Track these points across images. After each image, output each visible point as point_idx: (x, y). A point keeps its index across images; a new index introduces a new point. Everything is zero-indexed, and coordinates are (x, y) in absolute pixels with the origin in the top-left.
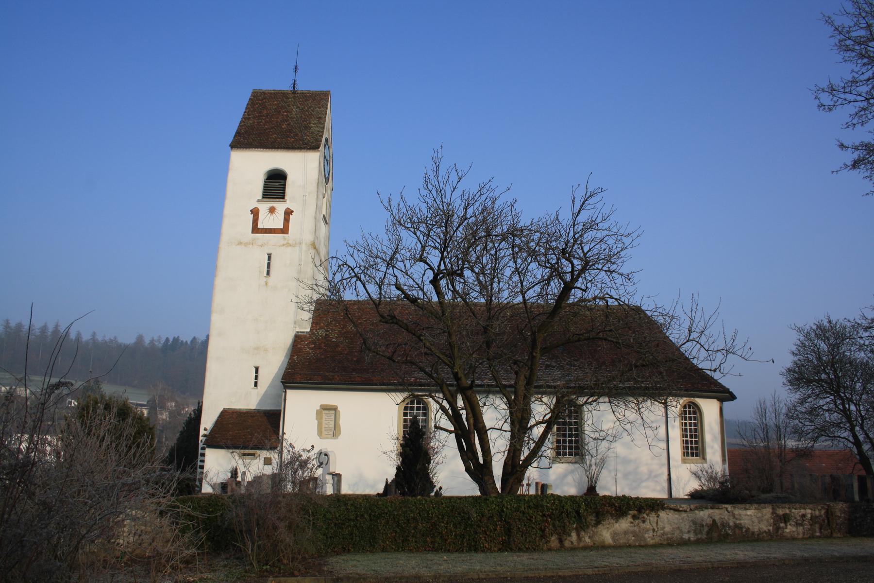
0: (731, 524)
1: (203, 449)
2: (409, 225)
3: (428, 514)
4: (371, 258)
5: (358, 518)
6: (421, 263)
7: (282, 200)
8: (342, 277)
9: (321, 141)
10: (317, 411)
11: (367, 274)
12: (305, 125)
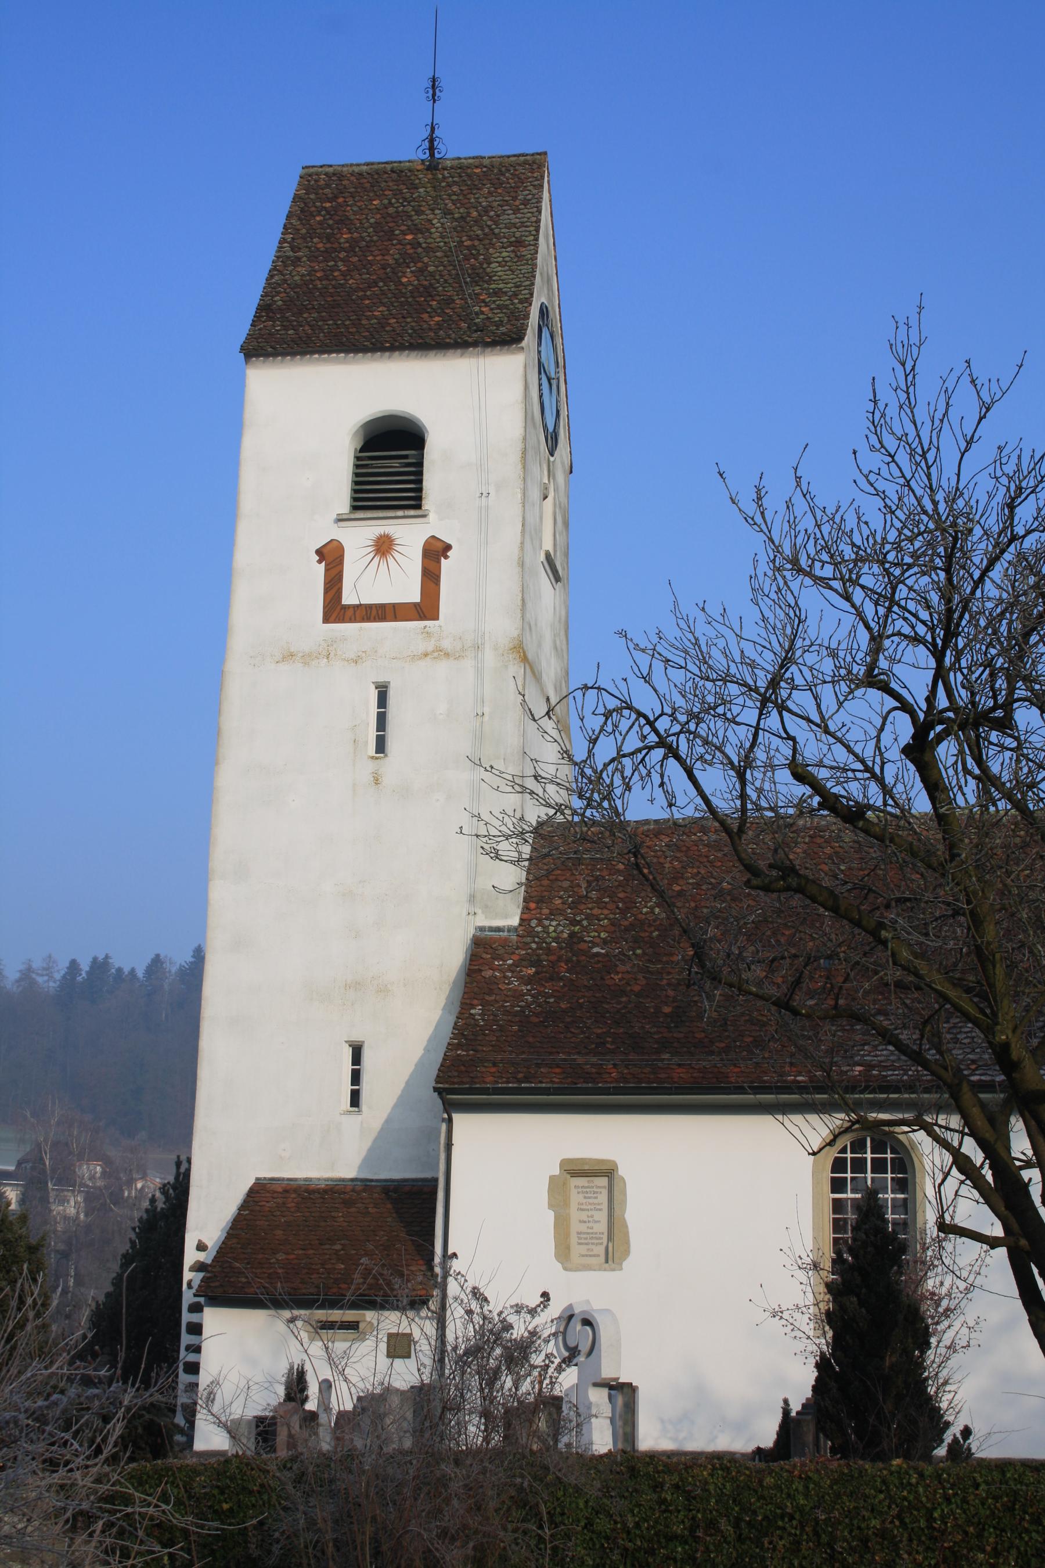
1: (196, 1308)
2: (828, 571)
3: (930, 1519)
4: (709, 685)
5: (700, 1533)
6: (870, 690)
7: (412, 512)
8: (619, 749)
9: (527, 316)
10: (552, 1178)
11: (696, 735)
12: (473, 268)
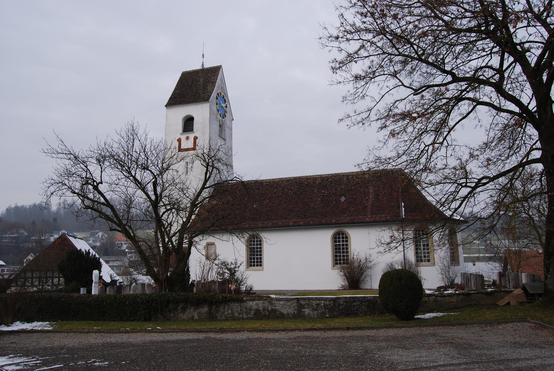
0: (269, 309)
